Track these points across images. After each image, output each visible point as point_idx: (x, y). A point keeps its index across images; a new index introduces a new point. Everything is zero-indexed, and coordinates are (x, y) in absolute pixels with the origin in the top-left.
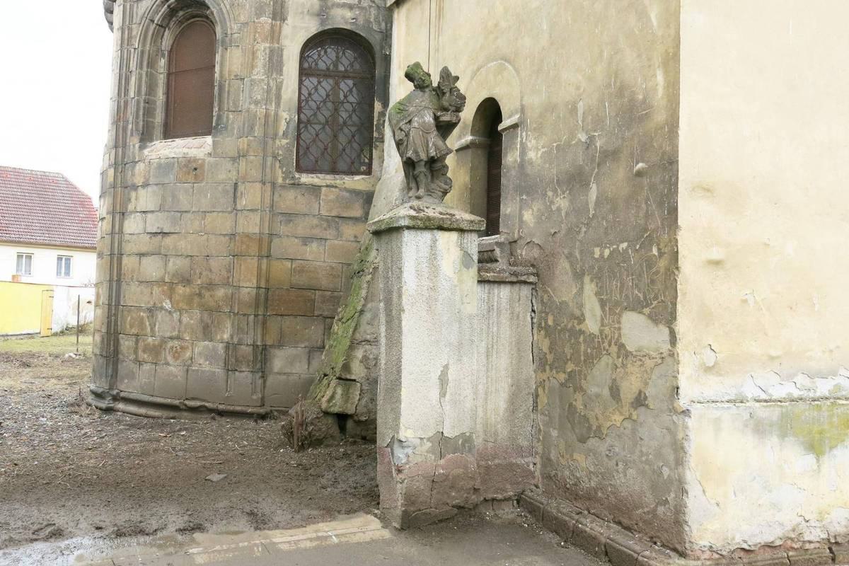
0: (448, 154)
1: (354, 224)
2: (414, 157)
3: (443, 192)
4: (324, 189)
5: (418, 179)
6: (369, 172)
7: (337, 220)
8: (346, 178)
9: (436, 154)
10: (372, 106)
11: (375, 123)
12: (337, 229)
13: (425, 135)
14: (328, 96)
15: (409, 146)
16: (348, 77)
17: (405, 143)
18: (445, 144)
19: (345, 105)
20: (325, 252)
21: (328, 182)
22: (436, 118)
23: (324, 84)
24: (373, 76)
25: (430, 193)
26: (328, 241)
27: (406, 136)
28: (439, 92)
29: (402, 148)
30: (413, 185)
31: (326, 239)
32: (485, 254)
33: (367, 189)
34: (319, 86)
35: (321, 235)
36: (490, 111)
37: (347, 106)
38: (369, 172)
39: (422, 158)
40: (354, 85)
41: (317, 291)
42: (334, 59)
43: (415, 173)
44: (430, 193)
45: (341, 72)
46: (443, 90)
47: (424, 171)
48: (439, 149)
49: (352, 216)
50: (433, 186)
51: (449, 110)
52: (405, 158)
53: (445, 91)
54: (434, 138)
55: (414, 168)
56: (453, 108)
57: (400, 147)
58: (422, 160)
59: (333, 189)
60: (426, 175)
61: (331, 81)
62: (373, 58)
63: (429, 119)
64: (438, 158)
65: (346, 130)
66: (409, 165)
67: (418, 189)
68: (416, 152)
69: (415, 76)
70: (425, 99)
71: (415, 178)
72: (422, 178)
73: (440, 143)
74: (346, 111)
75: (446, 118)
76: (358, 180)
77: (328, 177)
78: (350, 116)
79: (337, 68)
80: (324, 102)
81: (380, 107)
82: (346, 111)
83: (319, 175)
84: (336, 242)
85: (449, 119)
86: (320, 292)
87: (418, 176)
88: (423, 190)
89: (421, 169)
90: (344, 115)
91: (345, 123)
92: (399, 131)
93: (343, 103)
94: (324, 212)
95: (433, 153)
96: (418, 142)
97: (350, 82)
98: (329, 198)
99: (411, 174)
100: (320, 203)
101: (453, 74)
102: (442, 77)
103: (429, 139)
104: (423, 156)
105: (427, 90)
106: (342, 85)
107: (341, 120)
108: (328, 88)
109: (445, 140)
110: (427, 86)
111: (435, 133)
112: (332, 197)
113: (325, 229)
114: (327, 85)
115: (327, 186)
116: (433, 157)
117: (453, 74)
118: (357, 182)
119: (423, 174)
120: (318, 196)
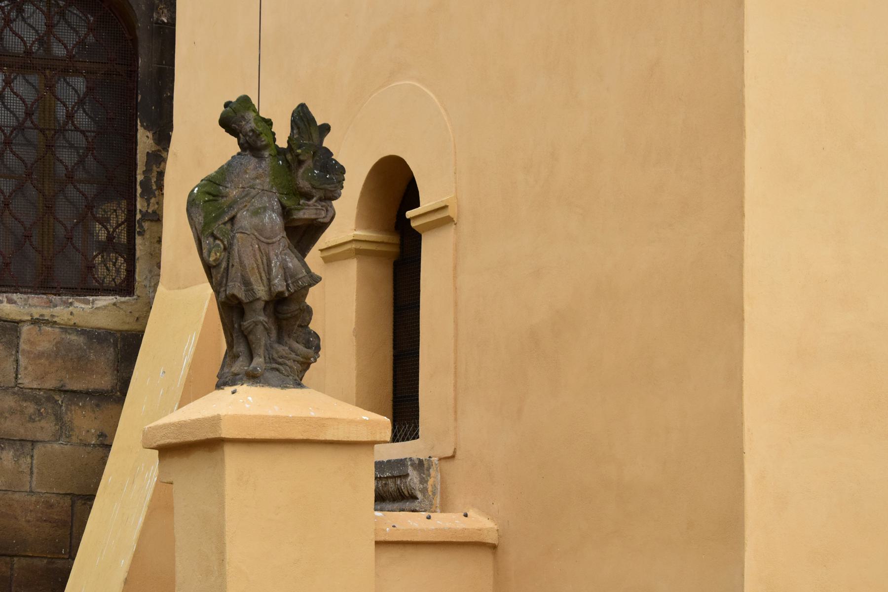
0: (310, 285)
1: (97, 406)
2: (241, 294)
3: (302, 363)
4: (25, 329)
5: (251, 337)
6: (126, 288)
7: (59, 398)
8: (76, 304)
9: (288, 286)
10: (133, 141)
11: (140, 178)
12: (59, 418)
13: (263, 246)
14: (29, 114)
15: (232, 271)
16: (77, 72)
17: (224, 265)
18: (305, 265)
19: (69, 134)
20: (32, 473)
21: (36, 312)
22: (286, 213)
23: (20, 85)
24: (132, 73)
25: (275, 366)
26: (39, 446)
27: (225, 249)
28: (289, 159)
29: (218, 275)
30: (241, 348)
31: (33, 442)
32: (390, 482)
33: (126, 327)
34: (8, 90)
35: (22, 433)
36: (395, 186)
37: (78, 139)
38: (126, 288)
39: (258, 295)
40: (89, 89)
41: (16, 559)
42: (42, 29)
43: (245, 324)
44: (275, 366)
45: (57, 59)
46: (298, 155)
47: (264, 330)
48: (292, 276)
49: (92, 387)
50: (282, 349)
51: (312, 197)
52: (223, 295)
53: (301, 158)
54: (281, 255)
55: (242, 314)
56: (320, 194)
57: (214, 271)
58: (259, 299)
59: (48, 329)
60: (266, 329)
61: (34, 78)
62: (132, 29)
63: (273, 219)
64: (291, 294)
65: (70, 190)
66: (232, 310)
67: (251, 358)
68: (247, 283)
69: (236, 118)
70: (259, 172)
71: (245, 336)
72: (261, 339)
73: (292, 262)
74: (71, 146)
75: (306, 213)
76: (105, 307)
77: (34, 299)
78: (81, 161)
79: (48, 50)
80: (20, 128)
81: (150, 141)
82: (71, 146)
83: (15, 296)
84: (56, 446)
85: (313, 217)
86: (24, 561)
87: (250, 332)
88: (261, 360)
89: (259, 318)
90: (68, 157)
91: (70, 177)
92: (211, 240)
93: (62, 130)
94: (26, 381)
95: (279, 285)
96: (249, 262)
97: (80, 84)
98: (39, 348)
99: (236, 326)
100: (17, 361)
101: (319, 123)
102: (294, 123)
103: (272, 254)
104: (261, 291)
105: (266, 154)
106: (61, 88)
107: (61, 171)
108: (30, 96)
109: (304, 256)
110: (266, 147)
111: (286, 241)
112: (45, 345)
113: (31, 420)
114: (24, 88)
115: (35, 322)
116: (281, 293)
117: (319, 123)
118: (99, 311)
119: (260, 328)
120: (14, 345)
